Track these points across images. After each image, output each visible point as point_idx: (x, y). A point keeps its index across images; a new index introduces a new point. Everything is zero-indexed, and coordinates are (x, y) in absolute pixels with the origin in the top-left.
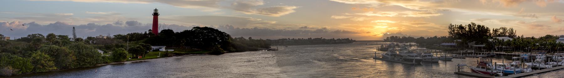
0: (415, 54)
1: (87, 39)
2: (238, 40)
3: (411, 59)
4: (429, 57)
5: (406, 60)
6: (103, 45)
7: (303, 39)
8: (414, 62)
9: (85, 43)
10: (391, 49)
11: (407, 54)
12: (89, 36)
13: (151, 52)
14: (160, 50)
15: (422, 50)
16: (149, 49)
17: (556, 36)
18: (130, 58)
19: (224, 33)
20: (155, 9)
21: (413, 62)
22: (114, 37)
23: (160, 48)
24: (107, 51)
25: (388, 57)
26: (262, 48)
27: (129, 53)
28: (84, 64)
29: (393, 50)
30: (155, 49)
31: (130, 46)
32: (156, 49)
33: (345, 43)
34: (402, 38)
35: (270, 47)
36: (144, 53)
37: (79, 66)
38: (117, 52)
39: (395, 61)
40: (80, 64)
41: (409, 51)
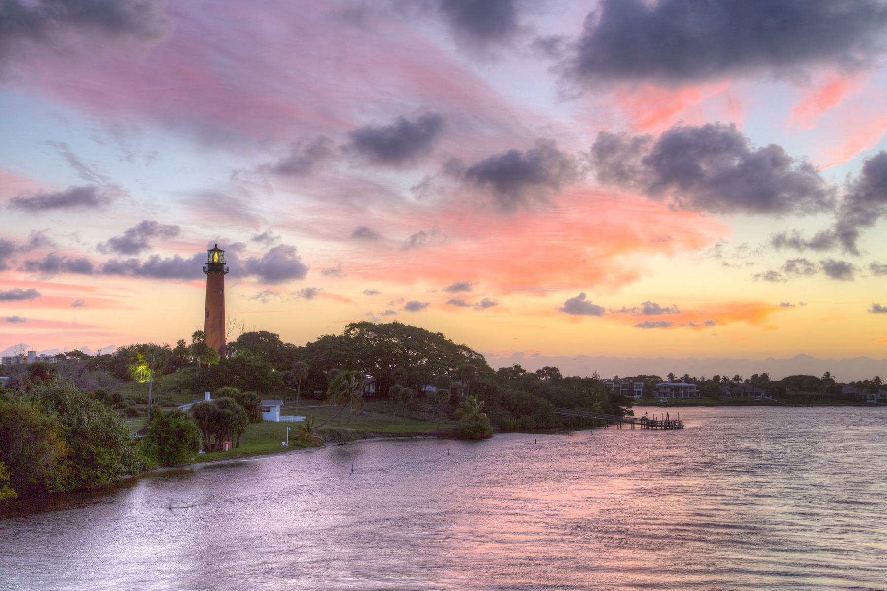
17: (587, 378)
19: (463, 347)
20: (214, 247)
35: (631, 413)
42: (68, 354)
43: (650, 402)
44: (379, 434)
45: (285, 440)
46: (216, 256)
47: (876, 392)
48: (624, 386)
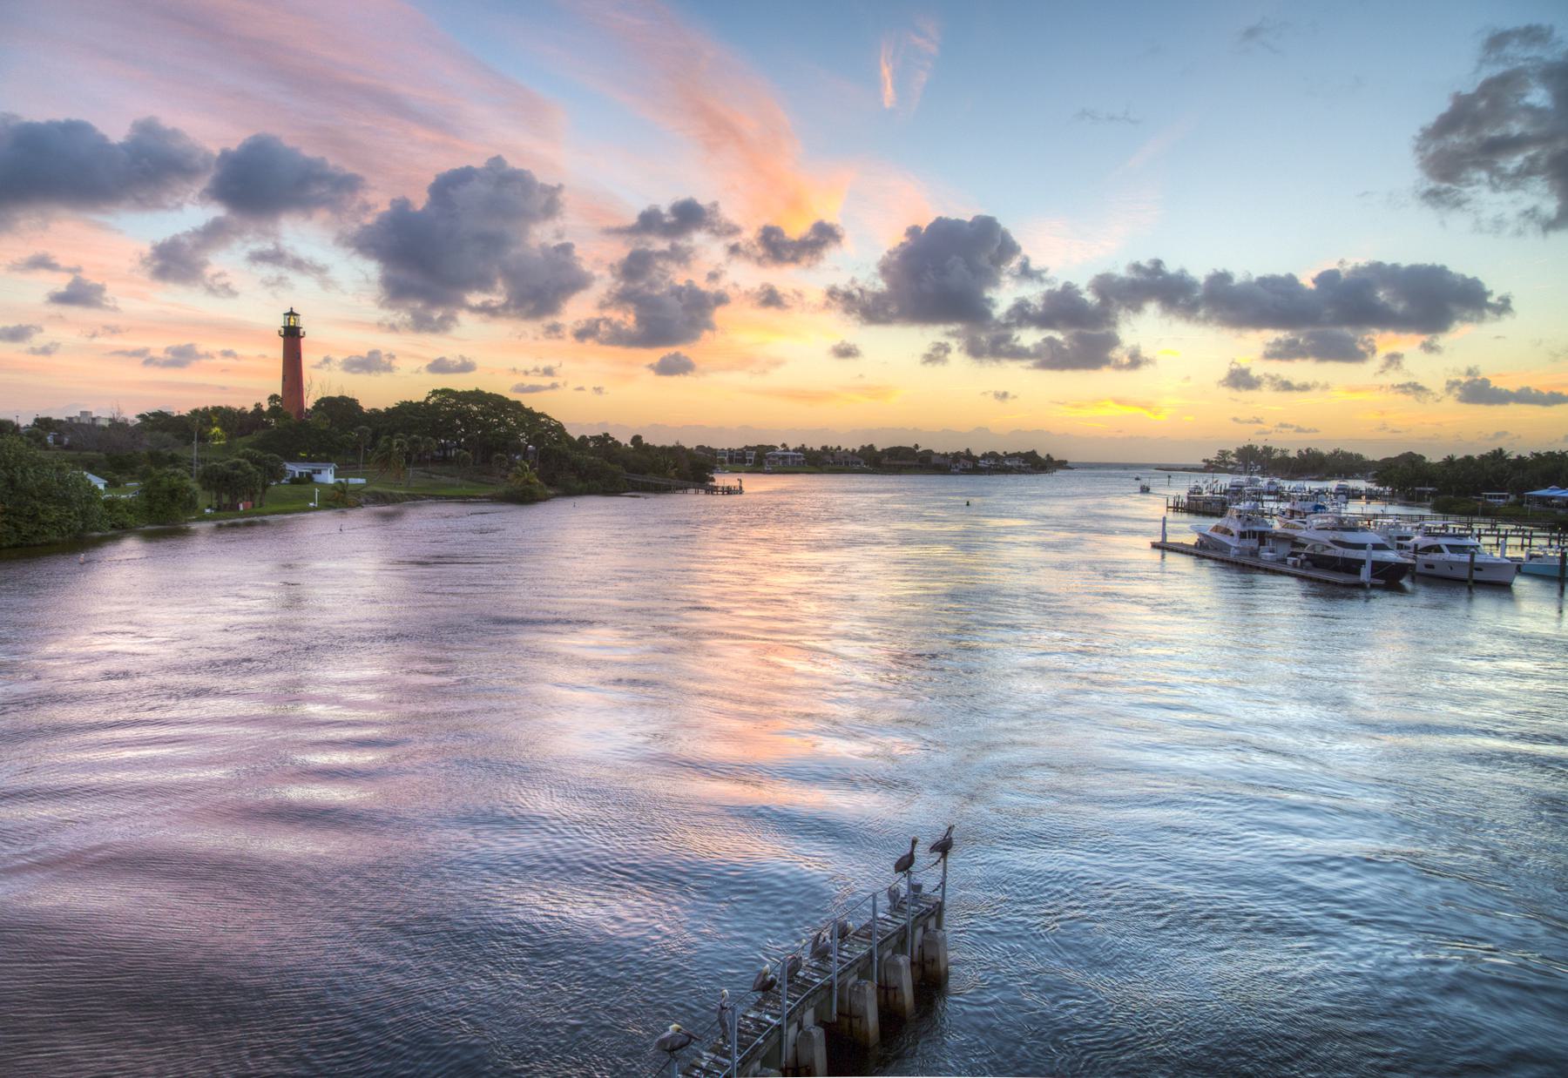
0: (1371, 538)
1: (34, 425)
2: (591, 445)
3: (1345, 560)
4: (1455, 557)
5: (1319, 562)
6: (103, 455)
7: (839, 448)
8: (1365, 575)
9: (28, 444)
10: (1245, 506)
11: (1328, 532)
12: (43, 415)
13: (278, 487)
14: (317, 478)
15: (1410, 518)
16: (275, 473)
18: (209, 507)
19: (542, 415)
20: (289, 311)
21: (1358, 573)
22: (139, 421)
23: (314, 472)
24: (118, 476)
25: (1230, 546)
26: (686, 483)
27: (204, 489)
28: (37, 531)
29: (1254, 510)
30: (297, 475)
31: (203, 461)
32: (301, 474)
33: (1020, 471)
34: (1296, 455)
35: (713, 480)
36: (260, 490)
37: (14, 540)
38: (158, 483)
39: (1261, 565)
40: (18, 530)
41: (1341, 520)
42: (150, 414)
43: (759, 469)
44: (430, 496)
45: (314, 501)
46: (292, 320)
47: (958, 461)
48: (737, 454)
